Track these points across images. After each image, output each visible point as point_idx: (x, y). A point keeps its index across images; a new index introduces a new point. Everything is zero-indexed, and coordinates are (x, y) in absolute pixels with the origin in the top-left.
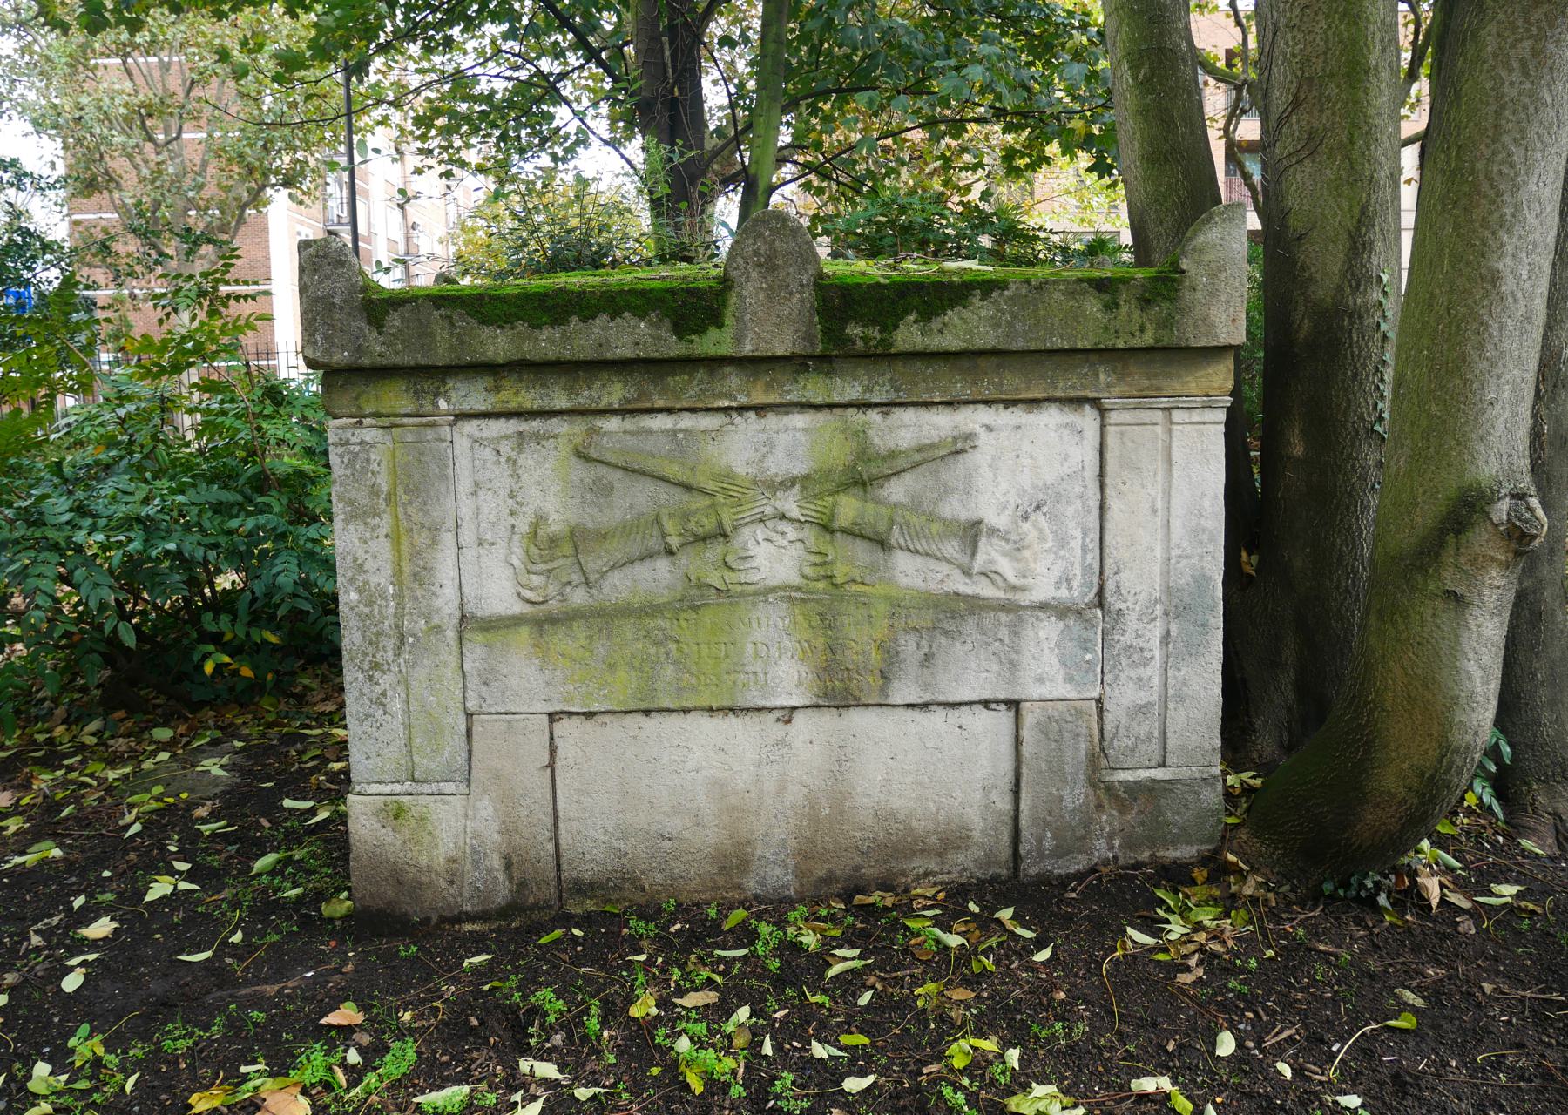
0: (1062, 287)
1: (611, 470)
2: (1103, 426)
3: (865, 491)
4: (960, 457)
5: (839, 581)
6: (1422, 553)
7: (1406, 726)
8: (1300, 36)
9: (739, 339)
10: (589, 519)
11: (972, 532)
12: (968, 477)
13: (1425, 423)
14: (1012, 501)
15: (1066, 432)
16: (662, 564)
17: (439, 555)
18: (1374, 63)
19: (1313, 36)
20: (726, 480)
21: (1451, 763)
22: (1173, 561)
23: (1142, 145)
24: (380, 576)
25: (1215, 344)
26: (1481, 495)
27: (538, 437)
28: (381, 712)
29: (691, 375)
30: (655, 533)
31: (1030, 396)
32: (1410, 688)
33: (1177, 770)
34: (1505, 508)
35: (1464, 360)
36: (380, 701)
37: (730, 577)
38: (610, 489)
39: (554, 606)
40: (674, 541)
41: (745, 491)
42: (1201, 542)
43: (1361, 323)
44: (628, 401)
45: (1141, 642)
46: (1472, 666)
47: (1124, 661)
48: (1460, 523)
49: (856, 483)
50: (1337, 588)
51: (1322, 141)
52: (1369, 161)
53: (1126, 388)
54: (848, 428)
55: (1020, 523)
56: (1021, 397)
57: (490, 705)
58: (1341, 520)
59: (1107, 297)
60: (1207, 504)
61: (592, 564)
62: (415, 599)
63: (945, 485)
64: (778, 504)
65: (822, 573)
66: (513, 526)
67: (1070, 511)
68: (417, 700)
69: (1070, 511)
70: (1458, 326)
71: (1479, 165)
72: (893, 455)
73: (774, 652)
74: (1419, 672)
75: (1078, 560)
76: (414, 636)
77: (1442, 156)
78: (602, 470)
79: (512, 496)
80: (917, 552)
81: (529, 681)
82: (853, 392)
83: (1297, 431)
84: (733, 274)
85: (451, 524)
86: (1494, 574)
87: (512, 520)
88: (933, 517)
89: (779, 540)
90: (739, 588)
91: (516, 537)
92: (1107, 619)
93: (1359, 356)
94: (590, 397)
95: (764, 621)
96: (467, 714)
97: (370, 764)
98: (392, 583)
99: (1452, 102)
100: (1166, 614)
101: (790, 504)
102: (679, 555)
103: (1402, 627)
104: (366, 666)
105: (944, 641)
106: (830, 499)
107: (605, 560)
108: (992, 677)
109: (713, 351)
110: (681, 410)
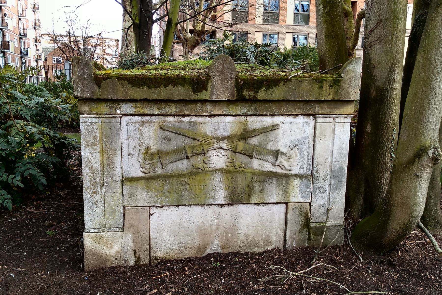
0: (307, 81)
1: (171, 133)
2: (315, 123)
3: (246, 141)
4: (274, 131)
5: (237, 167)
6: (409, 163)
7: (401, 210)
8: (379, 6)
9: (212, 94)
10: (163, 148)
11: (276, 154)
12: (276, 138)
13: (412, 128)
14: (288, 145)
15: (305, 124)
16: (185, 162)
17: (116, 158)
18: (400, 16)
19: (383, 6)
20: (205, 137)
21: (412, 220)
22: (333, 163)
23: (325, 33)
24: (97, 164)
25: (350, 99)
26: (426, 148)
27: (147, 122)
28: (95, 207)
29: (196, 105)
30: (184, 153)
31: (295, 113)
32: (403, 200)
33: (331, 223)
34: (432, 152)
35: (424, 110)
36: (95, 203)
37: (205, 166)
38: (170, 139)
39: (152, 174)
40: (189, 155)
41: (211, 140)
42: (342, 157)
43: (390, 93)
44: (177, 112)
45: (323, 186)
46: (419, 194)
47: (318, 191)
48: (420, 155)
49: (243, 139)
50: (378, 171)
51: (383, 38)
52: (396, 45)
53: (323, 112)
54: (241, 122)
55: (290, 151)
56: (293, 114)
57: (131, 204)
58: (380, 151)
59: (320, 84)
60: (344, 146)
61: (164, 162)
62: (108, 172)
63: (269, 139)
64: (221, 145)
65: (232, 165)
66: (140, 150)
67: (305, 147)
68: (107, 203)
69: (305, 147)
70: (423, 101)
71: (433, 56)
72: (254, 130)
73: (217, 188)
74: (405, 196)
75: (306, 162)
76: (107, 183)
77: (423, 53)
78: (168, 133)
79: (139, 140)
80: (260, 159)
81: (144, 197)
82: (244, 111)
83: (369, 124)
84: (211, 74)
85: (120, 148)
86: (428, 169)
87: (139, 148)
88: (265, 149)
89: (220, 155)
90: (208, 169)
91: (141, 153)
92: (314, 179)
93: (389, 103)
94: (165, 111)
95: (215, 179)
96: (123, 207)
97: (91, 223)
98: (100, 167)
99: (427, 37)
100: (331, 178)
101: (224, 144)
102: (190, 159)
103: (401, 183)
104: (91, 193)
105: (267, 185)
106: (235, 143)
107: (168, 160)
108: (280, 196)
109: (204, 98)
110: (192, 115)
